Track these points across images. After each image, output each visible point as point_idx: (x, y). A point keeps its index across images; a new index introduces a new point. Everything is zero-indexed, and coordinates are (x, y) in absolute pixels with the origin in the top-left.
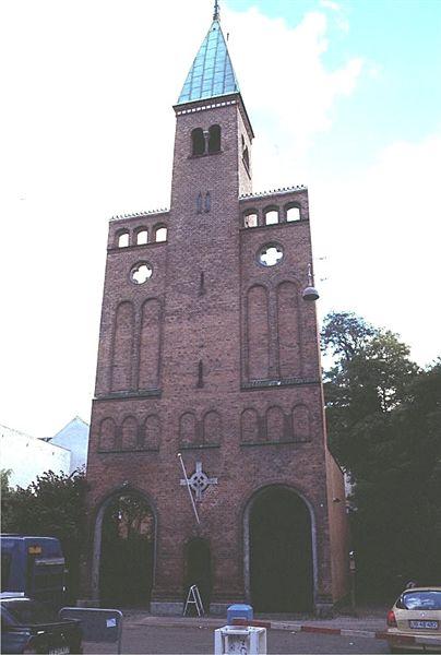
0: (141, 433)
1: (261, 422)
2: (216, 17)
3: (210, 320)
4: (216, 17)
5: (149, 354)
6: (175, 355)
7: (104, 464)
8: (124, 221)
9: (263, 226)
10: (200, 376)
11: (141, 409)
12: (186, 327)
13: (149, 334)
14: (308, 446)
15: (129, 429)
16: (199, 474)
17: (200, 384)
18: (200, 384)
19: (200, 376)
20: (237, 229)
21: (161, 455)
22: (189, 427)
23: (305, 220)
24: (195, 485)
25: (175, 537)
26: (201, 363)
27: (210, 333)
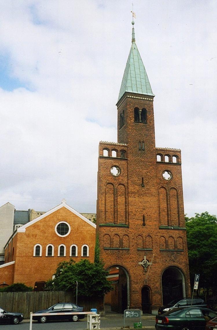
0: (121, 243)
1: (166, 242)
2: (133, 40)
3: (147, 199)
4: (133, 40)
5: (121, 208)
6: (134, 211)
7: (107, 254)
8: (108, 144)
9: (163, 162)
10: (144, 220)
11: (120, 231)
12: (137, 200)
13: (121, 200)
14: (182, 253)
15: (116, 240)
16: (145, 260)
17: (144, 224)
18: (144, 224)
19: (144, 220)
20: (52, 225)
21: (130, 252)
22: (140, 241)
23: (179, 164)
24: (144, 265)
25: (137, 285)
26: (144, 216)
27: (146, 204)
